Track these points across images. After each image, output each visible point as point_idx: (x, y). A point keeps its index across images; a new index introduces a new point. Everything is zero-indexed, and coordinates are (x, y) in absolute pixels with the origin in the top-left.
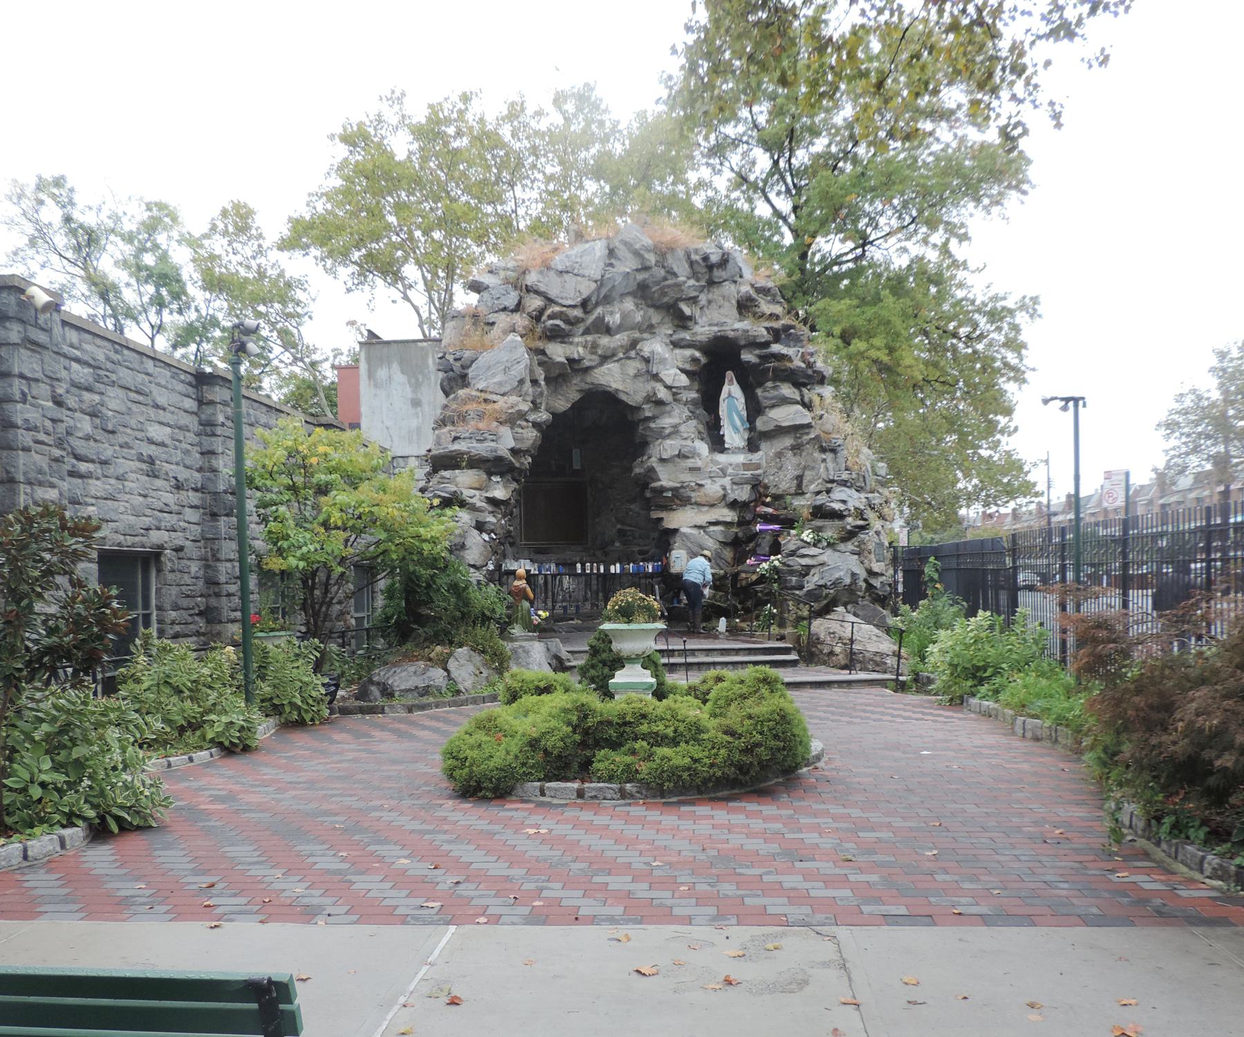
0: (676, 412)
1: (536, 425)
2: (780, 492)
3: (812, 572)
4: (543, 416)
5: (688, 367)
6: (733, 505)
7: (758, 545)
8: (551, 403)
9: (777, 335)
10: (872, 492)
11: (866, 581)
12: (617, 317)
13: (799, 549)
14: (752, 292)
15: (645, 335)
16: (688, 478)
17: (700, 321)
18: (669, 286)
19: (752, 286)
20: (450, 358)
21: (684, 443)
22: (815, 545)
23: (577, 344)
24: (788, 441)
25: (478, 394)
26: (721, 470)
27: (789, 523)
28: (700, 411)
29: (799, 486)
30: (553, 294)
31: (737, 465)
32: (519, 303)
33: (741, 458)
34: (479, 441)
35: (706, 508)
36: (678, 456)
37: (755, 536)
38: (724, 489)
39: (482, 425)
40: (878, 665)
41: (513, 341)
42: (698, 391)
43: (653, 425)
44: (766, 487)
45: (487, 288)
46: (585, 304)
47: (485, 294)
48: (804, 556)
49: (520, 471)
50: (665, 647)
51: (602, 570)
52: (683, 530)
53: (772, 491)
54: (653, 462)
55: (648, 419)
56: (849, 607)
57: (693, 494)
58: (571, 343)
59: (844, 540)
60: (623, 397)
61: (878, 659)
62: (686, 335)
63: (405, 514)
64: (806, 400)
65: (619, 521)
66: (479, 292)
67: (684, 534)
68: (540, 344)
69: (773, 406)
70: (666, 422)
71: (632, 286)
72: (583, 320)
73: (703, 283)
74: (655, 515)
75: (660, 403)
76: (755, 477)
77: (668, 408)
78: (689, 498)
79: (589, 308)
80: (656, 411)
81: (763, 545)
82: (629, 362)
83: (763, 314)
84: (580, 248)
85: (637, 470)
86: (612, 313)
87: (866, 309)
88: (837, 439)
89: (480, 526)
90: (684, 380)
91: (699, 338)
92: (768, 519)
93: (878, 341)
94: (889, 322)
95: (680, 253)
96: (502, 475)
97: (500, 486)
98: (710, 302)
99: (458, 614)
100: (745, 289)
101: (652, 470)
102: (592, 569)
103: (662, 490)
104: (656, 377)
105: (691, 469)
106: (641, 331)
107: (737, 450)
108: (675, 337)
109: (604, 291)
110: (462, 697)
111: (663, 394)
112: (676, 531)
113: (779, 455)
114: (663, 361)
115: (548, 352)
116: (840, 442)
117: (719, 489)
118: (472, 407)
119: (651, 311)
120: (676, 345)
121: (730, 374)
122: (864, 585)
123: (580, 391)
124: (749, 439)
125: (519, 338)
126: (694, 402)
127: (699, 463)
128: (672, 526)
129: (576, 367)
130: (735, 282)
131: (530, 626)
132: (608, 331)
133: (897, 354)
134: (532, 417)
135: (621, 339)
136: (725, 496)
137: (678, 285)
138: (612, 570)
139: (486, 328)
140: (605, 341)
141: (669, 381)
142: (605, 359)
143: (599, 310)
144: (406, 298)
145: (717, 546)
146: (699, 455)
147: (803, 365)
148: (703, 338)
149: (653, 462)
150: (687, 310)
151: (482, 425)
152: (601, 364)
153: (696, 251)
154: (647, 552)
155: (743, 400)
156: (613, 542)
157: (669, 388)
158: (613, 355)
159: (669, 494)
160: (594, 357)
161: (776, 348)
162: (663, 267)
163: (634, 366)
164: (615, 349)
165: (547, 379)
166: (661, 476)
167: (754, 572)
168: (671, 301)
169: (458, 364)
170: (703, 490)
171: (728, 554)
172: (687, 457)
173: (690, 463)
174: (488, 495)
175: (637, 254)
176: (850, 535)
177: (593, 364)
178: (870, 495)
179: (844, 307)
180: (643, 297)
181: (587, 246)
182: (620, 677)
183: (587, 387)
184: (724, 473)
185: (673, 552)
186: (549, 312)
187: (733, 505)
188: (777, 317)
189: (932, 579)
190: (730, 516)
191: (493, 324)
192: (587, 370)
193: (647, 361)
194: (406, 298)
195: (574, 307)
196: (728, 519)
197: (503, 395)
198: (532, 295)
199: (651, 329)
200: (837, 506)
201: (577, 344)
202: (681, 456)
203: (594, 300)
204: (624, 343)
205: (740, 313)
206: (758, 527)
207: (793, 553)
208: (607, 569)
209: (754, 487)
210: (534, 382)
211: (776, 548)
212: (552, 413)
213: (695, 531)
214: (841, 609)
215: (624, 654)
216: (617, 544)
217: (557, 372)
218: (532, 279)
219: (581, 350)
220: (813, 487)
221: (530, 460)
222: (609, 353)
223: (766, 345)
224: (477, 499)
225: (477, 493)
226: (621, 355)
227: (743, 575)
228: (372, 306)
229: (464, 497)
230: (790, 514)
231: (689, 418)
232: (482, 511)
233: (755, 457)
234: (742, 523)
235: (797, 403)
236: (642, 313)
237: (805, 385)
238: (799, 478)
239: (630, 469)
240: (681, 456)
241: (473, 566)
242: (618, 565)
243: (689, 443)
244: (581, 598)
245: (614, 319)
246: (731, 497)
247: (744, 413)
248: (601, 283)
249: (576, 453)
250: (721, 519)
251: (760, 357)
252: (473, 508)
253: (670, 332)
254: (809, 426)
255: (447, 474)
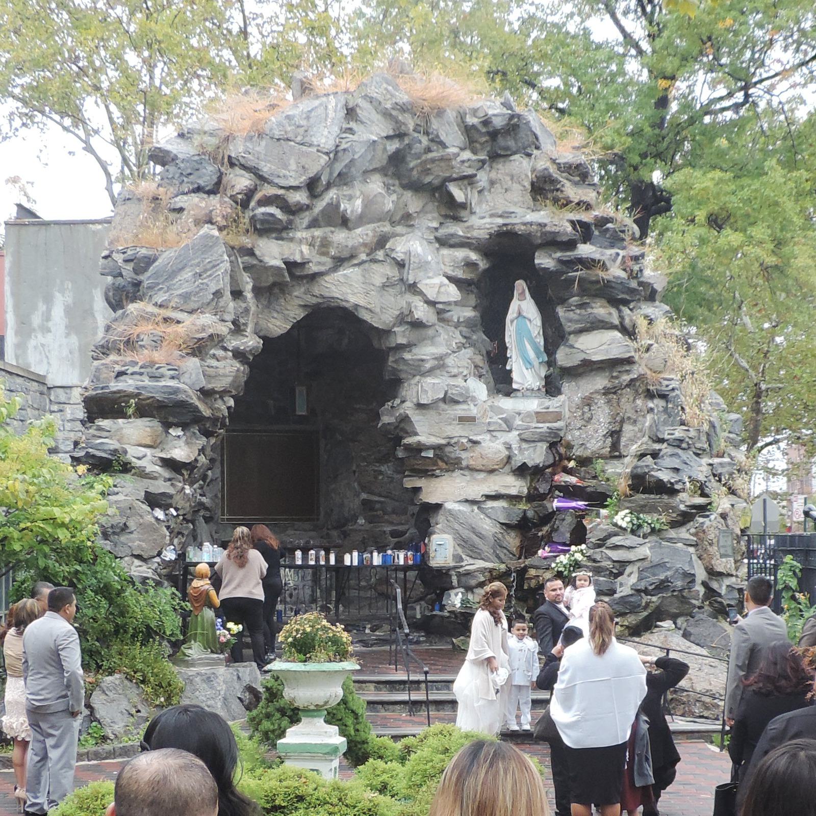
0: (443, 337)
1: (238, 355)
2: (588, 453)
3: (628, 570)
4: (250, 342)
5: (460, 274)
6: (522, 471)
7: (554, 530)
8: (263, 323)
9: (585, 232)
10: (721, 455)
11: (704, 584)
12: (358, 203)
13: (610, 536)
14: (553, 170)
15: (399, 229)
16: (457, 431)
17: (477, 209)
18: (433, 161)
19: (553, 161)
20: (119, 258)
21: (452, 382)
22: (633, 532)
23: (301, 241)
24: (600, 382)
25: (156, 310)
26: (505, 420)
27: (598, 499)
28: (479, 336)
29: (615, 446)
30: (266, 168)
31: (528, 415)
32: (219, 183)
33: (533, 405)
34: (153, 377)
35: (482, 475)
36: (444, 400)
37: (548, 518)
38: (509, 448)
39: (158, 356)
40: (707, 708)
41: (208, 237)
42: (475, 308)
43: (407, 356)
44: (569, 447)
45: (175, 158)
46: (312, 186)
47: (172, 168)
48: (616, 547)
49: (214, 420)
50: (405, 678)
51: (332, 561)
52: (449, 505)
53: (577, 452)
54: (408, 408)
55: (401, 347)
56: (680, 621)
57: (464, 455)
58: (291, 240)
59: (675, 524)
60: (365, 316)
61: (708, 700)
62: (457, 230)
63: (31, 488)
64: (627, 321)
65: (364, 488)
66: (163, 165)
67: (450, 511)
68: (246, 241)
69: (581, 331)
70: (427, 352)
71: (381, 159)
72: (308, 207)
73: (483, 156)
74: (409, 483)
75: (417, 325)
76: (554, 432)
77: (431, 332)
78: (458, 461)
79: (320, 189)
80: (413, 335)
81: (562, 529)
82: (375, 266)
83: (568, 202)
84: (306, 104)
85: (386, 419)
86: (350, 198)
87: (746, 181)
88: (671, 379)
89: (153, 500)
90: (453, 293)
91: (475, 234)
92: (570, 492)
93: (759, 232)
94: (776, 204)
95: (451, 115)
96: (185, 426)
97: (181, 443)
98: (492, 183)
99: (110, 627)
100: (542, 164)
101: (405, 419)
102: (317, 559)
103: (418, 449)
104: (413, 288)
105: (462, 419)
106: (393, 223)
107: (531, 392)
108: (442, 232)
109: (339, 167)
110: (107, 747)
111: (421, 312)
112: (438, 506)
113: (588, 402)
114: (423, 266)
115: (257, 252)
116: (673, 384)
117: (501, 448)
118: (146, 329)
119: (408, 194)
120: (443, 242)
121: (520, 285)
122: (702, 590)
123: (305, 306)
124: (547, 377)
125: (216, 233)
126: (470, 324)
127: (474, 411)
128: (433, 500)
129: (298, 273)
130: (529, 155)
131: (214, 645)
132: (345, 222)
133: (786, 250)
134: (234, 343)
135: (363, 234)
136: (509, 458)
137: (446, 160)
138: (347, 562)
139: (172, 216)
140: (340, 237)
141: (431, 296)
142: (340, 262)
143: (332, 194)
144: (89, 149)
145: (497, 529)
146: (474, 399)
147: (623, 275)
148: (483, 234)
149: (408, 408)
150: (459, 195)
151: (158, 356)
152: (335, 269)
153: (474, 112)
154: (403, 533)
155: (538, 322)
156: (354, 518)
157: (431, 303)
158: (352, 257)
159: (430, 454)
160: (324, 259)
161: (585, 250)
162: (427, 133)
163: (382, 272)
164: (354, 248)
165: (257, 291)
166: (418, 429)
167: (548, 568)
168: (436, 182)
169: (130, 267)
170: (478, 449)
171: (513, 541)
172: (457, 402)
173: (460, 410)
174: (163, 455)
175: (386, 114)
176: (685, 518)
177: (322, 269)
178: (716, 460)
179: (710, 184)
180: (397, 176)
181: (317, 103)
182: (294, 736)
183: (314, 301)
184: (509, 425)
185: (434, 537)
186: (258, 196)
187: (522, 471)
188: (588, 207)
189: (787, 588)
190: (516, 486)
191: (181, 210)
192: (313, 277)
193: (401, 265)
194: (89, 149)
195: (296, 188)
196: (514, 492)
197: (191, 312)
198: (238, 171)
199: (407, 219)
200: (665, 476)
201: (301, 241)
202: (448, 400)
203: (324, 179)
204: (368, 240)
205: (534, 199)
206: (556, 504)
207: (601, 543)
208: (340, 559)
209: (552, 446)
210: (237, 294)
211: (579, 535)
212: (264, 338)
213: (465, 508)
214: (667, 624)
215: (299, 704)
216: (361, 521)
217: (271, 280)
218: (236, 149)
219: (305, 249)
220: (634, 448)
221: (231, 403)
222: (346, 254)
223: (571, 245)
224: (147, 460)
225: (148, 451)
226: (363, 257)
227: (532, 572)
228: (44, 161)
229: (130, 457)
230: (602, 486)
231: (461, 346)
232: (155, 478)
233: (554, 404)
234: (533, 497)
235: (613, 327)
236: (394, 197)
237: (626, 303)
238: (615, 435)
239: (378, 417)
240: (448, 400)
241: (139, 557)
242: (355, 554)
243: (459, 381)
244: (307, 597)
245: (353, 206)
246: (518, 460)
247: (541, 341)
248: (336, 153)
249: (301, 393)
250: (504, 491)
251: (560, 261)
252: (143, 474)
253: (435, 224)
254: (629, 361)
255: (105, 423)
